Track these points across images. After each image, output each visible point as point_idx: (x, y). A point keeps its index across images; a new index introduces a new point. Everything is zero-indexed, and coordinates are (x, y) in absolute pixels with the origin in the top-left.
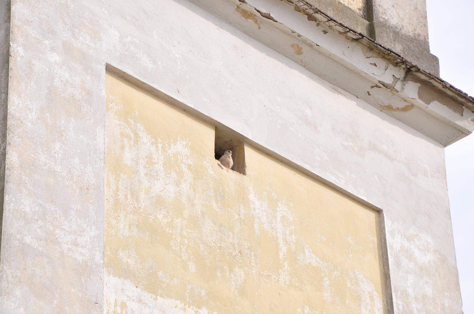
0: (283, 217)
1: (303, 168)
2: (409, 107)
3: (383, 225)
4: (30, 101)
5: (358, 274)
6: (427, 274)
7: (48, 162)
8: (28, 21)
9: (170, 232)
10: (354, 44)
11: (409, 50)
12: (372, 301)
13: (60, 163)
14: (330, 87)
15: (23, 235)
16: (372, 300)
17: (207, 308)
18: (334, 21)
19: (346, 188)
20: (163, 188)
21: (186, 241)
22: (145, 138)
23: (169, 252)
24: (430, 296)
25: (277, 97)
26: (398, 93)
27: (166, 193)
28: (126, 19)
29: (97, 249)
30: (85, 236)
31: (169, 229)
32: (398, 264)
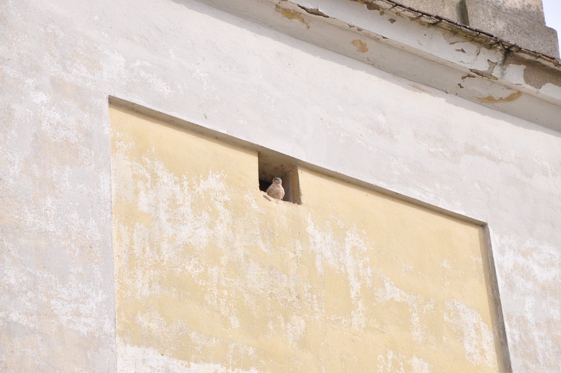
0: (354, 248)
1: (377, 186)
2: (516, 95)
3: (489, 242)
4: (11, 153)
5: (458, 305)
6: (552, 293)
7: (37, 222)
8: (3, 60)
9: (204, 284)
10: (432, 29)
11: (515, 26)
12: (479, 335)
13: (53, 221)
14: (410, 85)
15: (7, 312)
16: (478, 333)
17: (256, 368)
18: (401, 6)
19: (436, 203)
20: (192, 233)
21: (226, 293)
22: (165, 177)
23: (204, 308)
24: (557, 319)
25: (338, 107)
26: (498, 80)
27: (196, 239)
28: (133, 40)
29: (107, 316)
30: (89, 303)
31: (203, 281)
32: (511, 286)
